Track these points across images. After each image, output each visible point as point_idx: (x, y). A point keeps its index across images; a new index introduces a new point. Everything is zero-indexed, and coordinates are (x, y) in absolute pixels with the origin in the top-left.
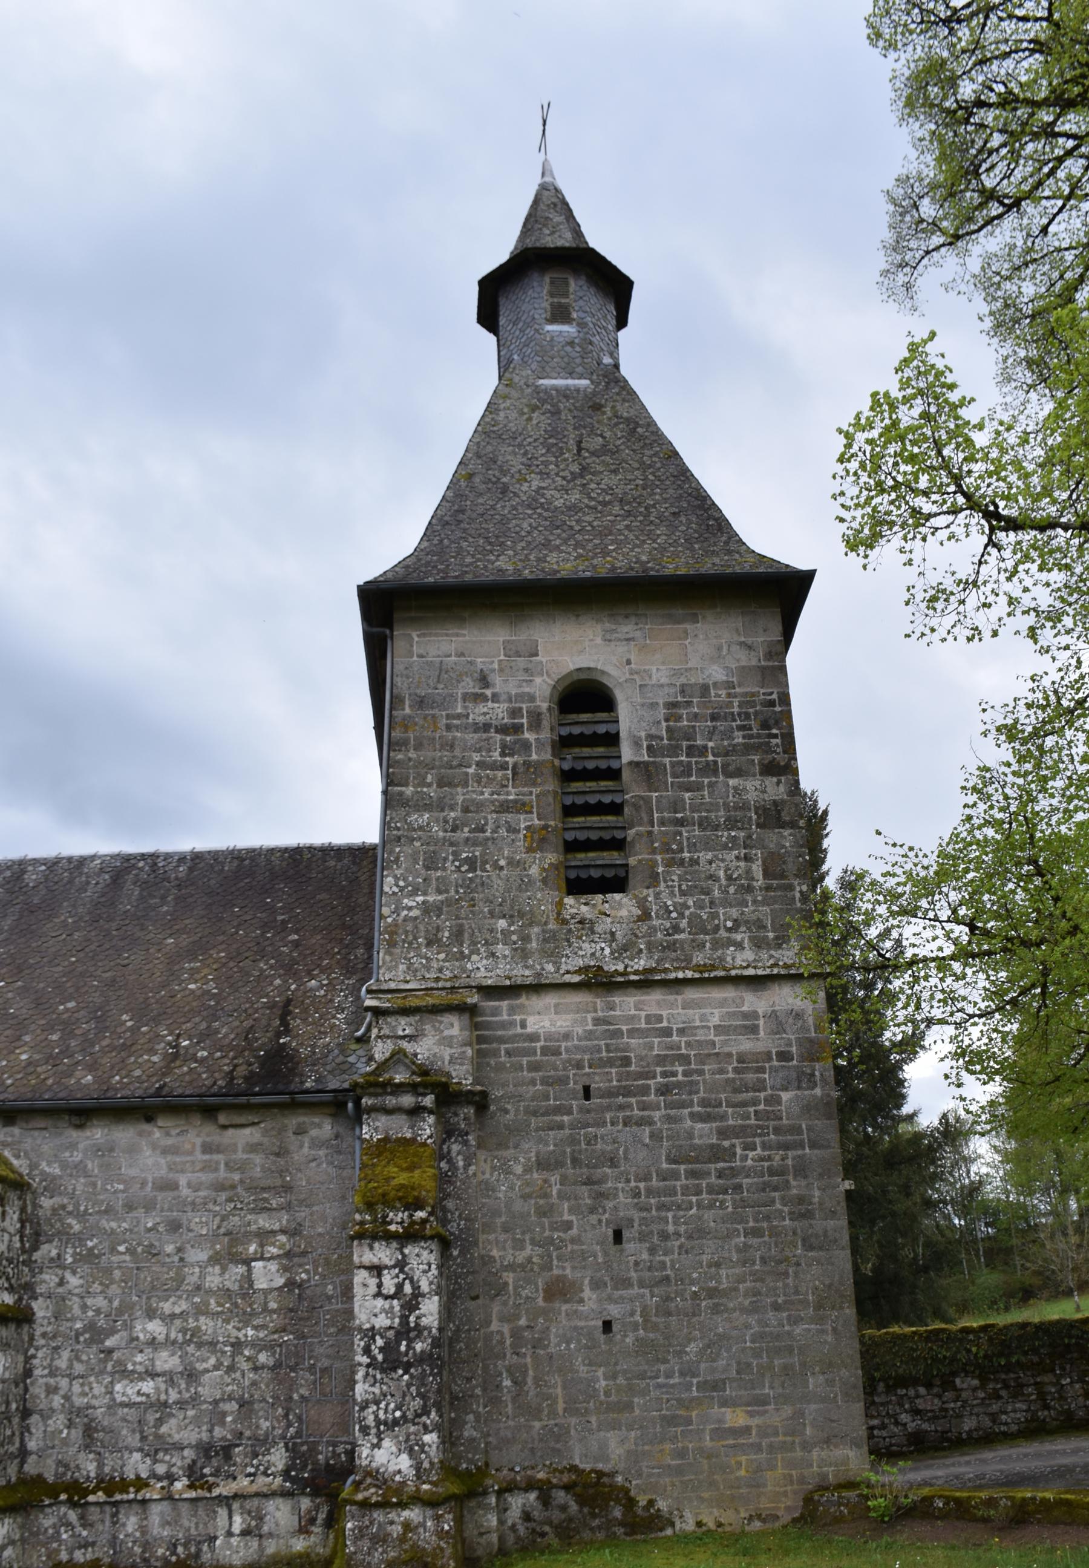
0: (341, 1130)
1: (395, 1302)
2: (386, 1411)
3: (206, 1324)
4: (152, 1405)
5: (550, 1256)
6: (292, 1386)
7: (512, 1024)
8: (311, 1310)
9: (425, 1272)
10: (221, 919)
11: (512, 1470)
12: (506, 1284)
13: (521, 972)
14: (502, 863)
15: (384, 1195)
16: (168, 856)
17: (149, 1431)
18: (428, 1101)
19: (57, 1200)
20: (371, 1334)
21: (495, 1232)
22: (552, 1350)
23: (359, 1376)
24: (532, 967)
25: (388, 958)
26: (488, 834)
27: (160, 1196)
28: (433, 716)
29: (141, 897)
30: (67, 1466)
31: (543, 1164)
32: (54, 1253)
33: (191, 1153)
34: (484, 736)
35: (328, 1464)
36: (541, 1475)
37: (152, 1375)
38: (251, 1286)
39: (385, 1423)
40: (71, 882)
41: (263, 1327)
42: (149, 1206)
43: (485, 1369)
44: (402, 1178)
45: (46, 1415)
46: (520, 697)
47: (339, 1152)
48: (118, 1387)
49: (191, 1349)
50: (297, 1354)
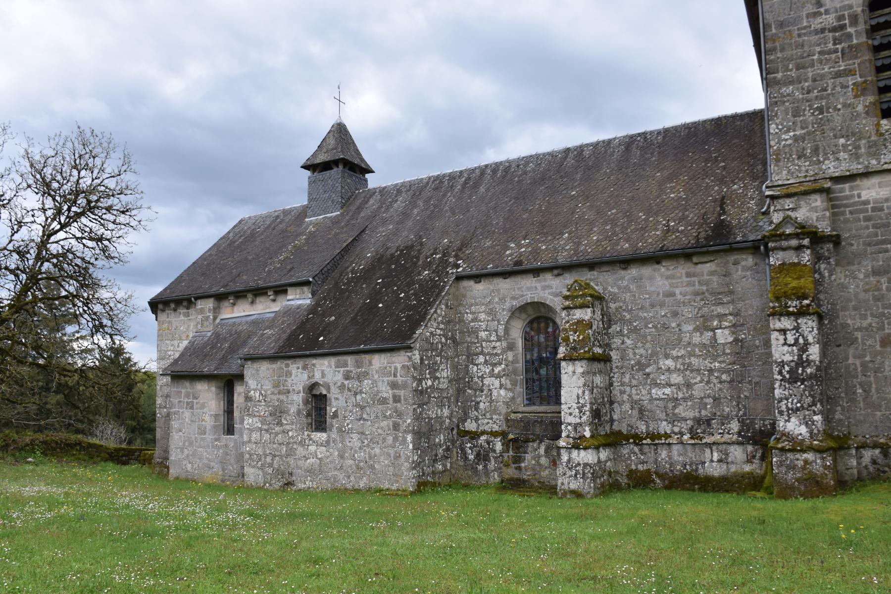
0: (758, 261)
1: (794, 348)
2: (792, 403)
3: (694, 361)
4: (670, 399)
5: (883, 323)
6: (740, 391)
7: (852, 196)
8: (748, 354)
9: (810, 332)
10: (683, 160)
11: (864, 437)
12: (857, 338)
13: (856, 167)
14: (839, 106)
15: (785, 293)
16: (651, 132)
17: (669, 412)
18: (806, 242)
19: (617, 304)
20: (782, 364)
21: (848, 310)
22: (886, 373)
23: (777, 385)
24: (862, 163)
25: (776, 168)
26: (829, 92)
27: (667, 300)
28: (790, 31)
29: (641, 155)
30: (632, 427)
31: (876, 272)
32: (618, 329)
33: (680, 278)
34: (822, 36)
35: (761, 430)
36: (882, 441)
37: (670, 385)
38: (716, 342)
39: (792, 410)
40: (606, 152)
41: (724, 362)
42: (662, 305)
43: (847, 383)
44: (794, 284)
45: (621, 404)
46: (843, 8)
47: (758, 273)
48: (653, 391)
49: (688, 373)
50: (742, 375)
